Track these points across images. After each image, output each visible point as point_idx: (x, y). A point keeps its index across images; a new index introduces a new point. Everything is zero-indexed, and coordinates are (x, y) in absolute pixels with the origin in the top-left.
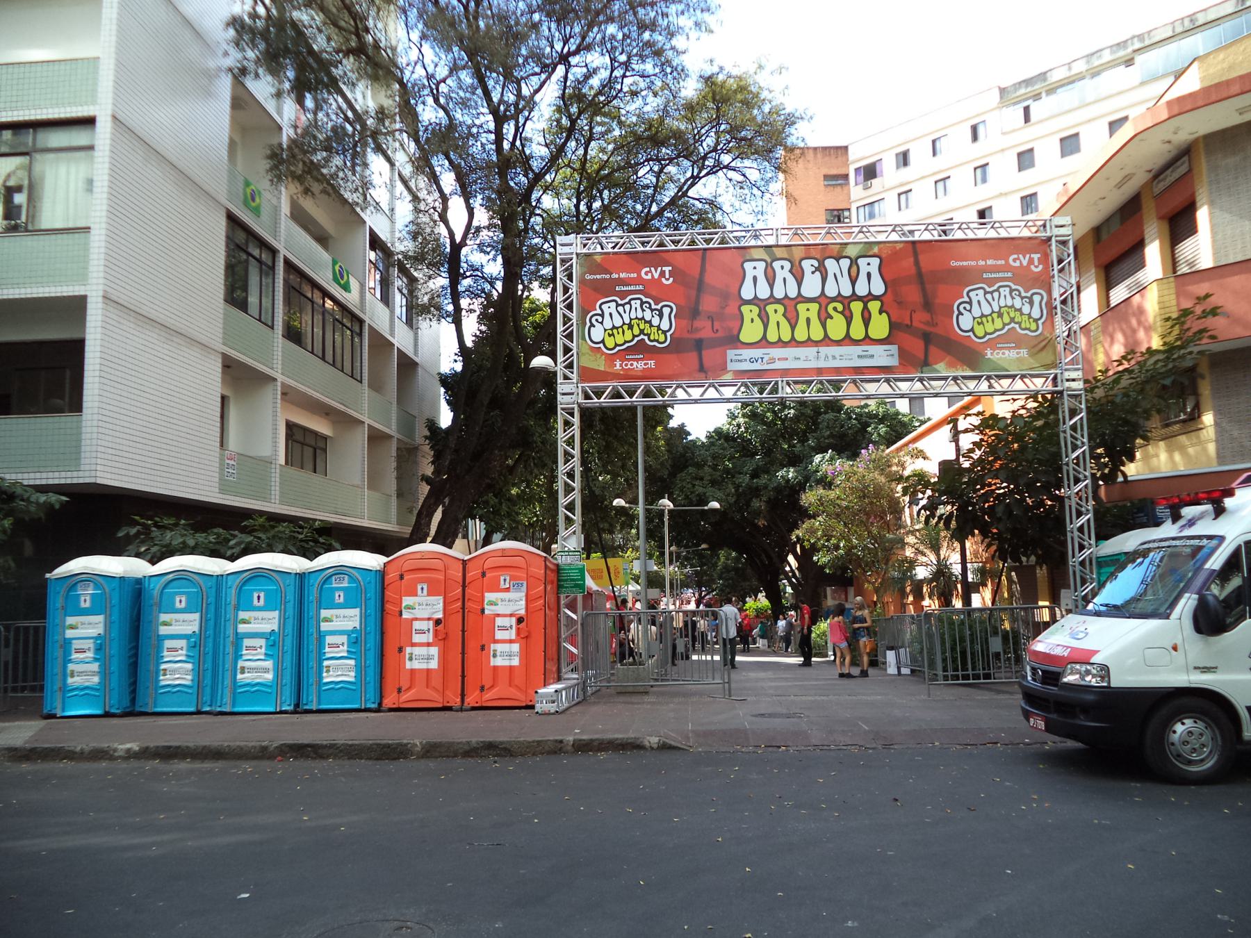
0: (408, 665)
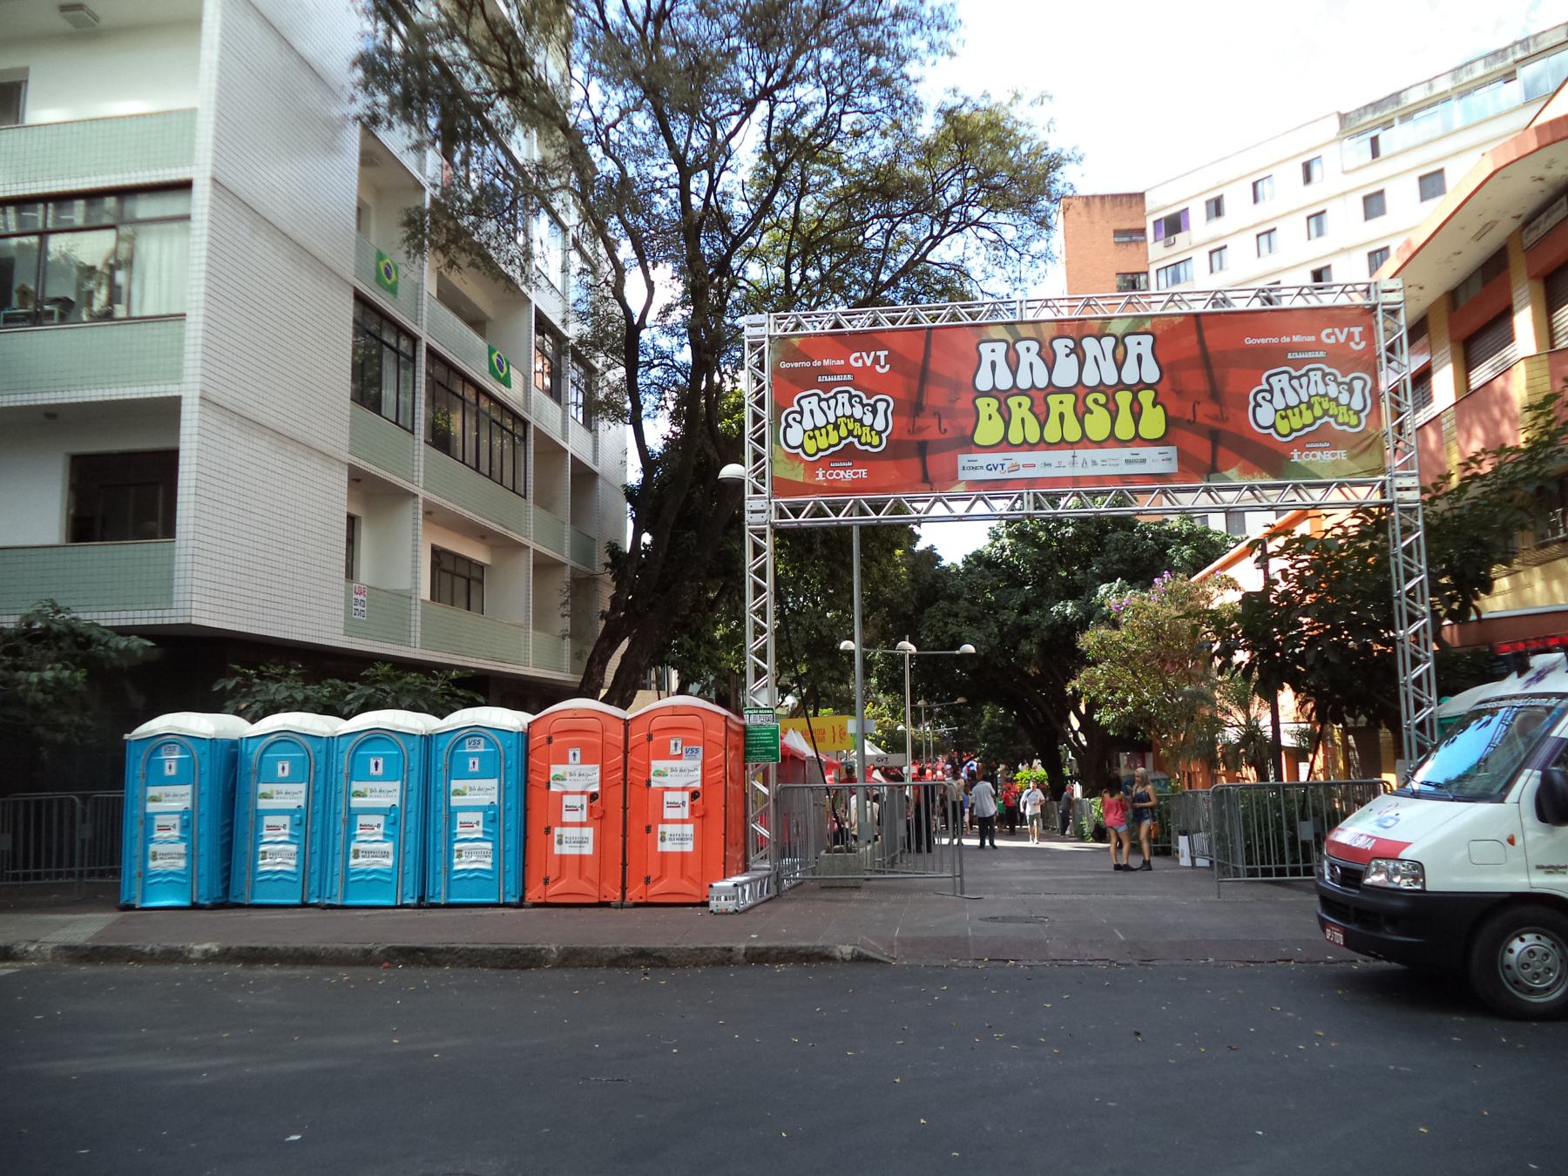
0: (557, 850)
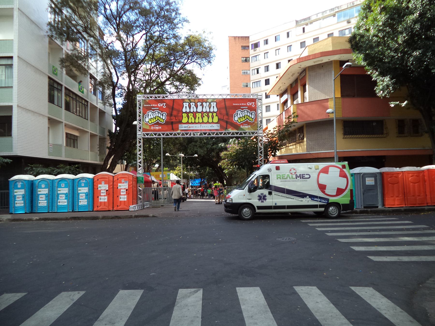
0: (100, 201)
